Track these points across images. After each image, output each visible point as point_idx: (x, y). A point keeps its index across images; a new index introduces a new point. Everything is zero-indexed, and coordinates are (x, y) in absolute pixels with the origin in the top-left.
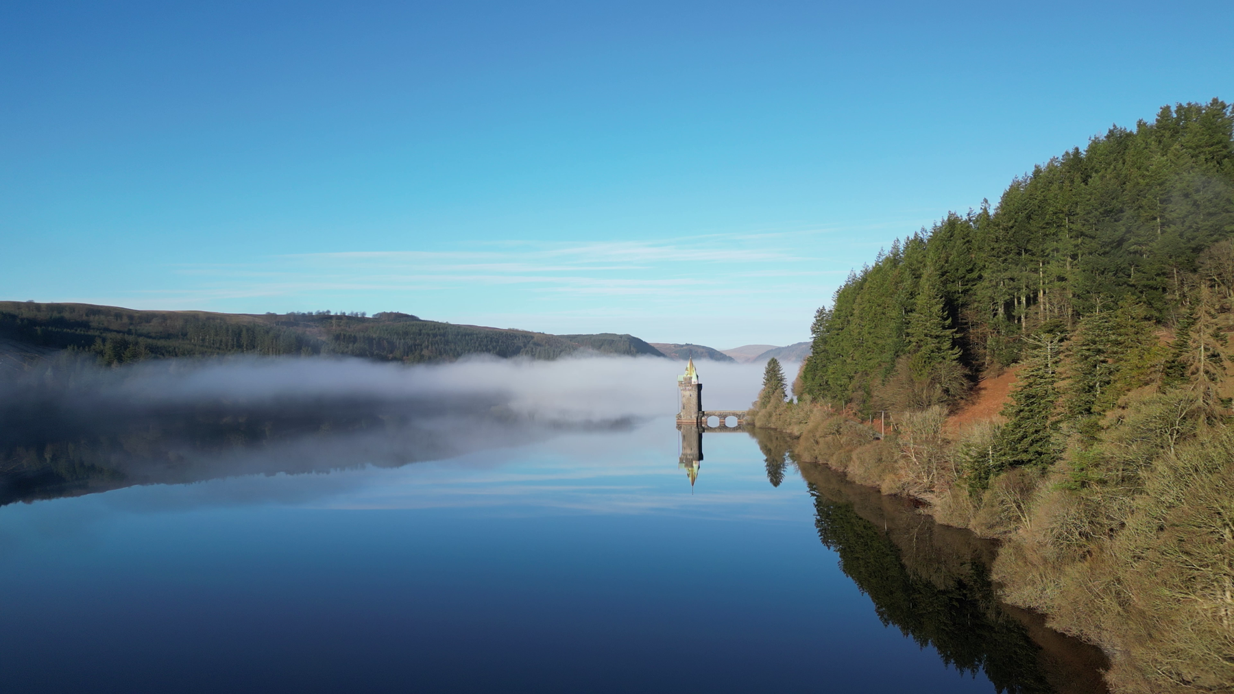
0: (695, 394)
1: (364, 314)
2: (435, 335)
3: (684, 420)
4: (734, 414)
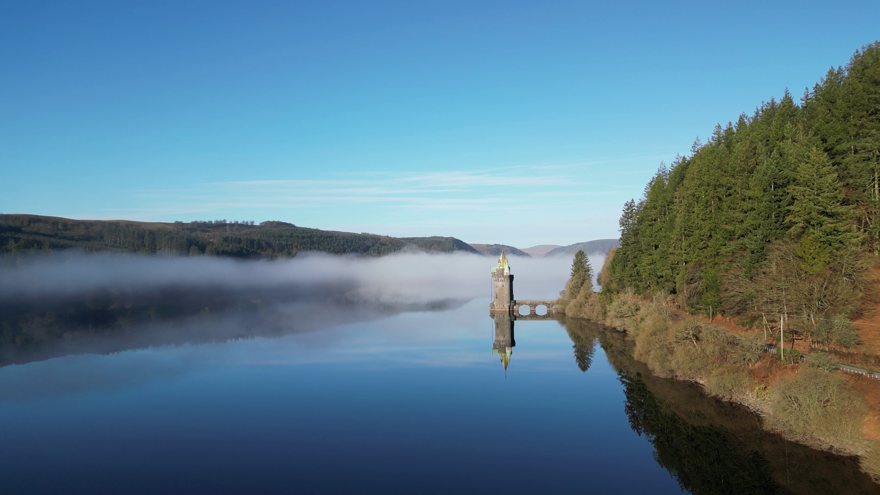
0: (507, 285)
1: (253, 222)
2: (303, 238)
3: (497, 308)
4: (544, 303)
